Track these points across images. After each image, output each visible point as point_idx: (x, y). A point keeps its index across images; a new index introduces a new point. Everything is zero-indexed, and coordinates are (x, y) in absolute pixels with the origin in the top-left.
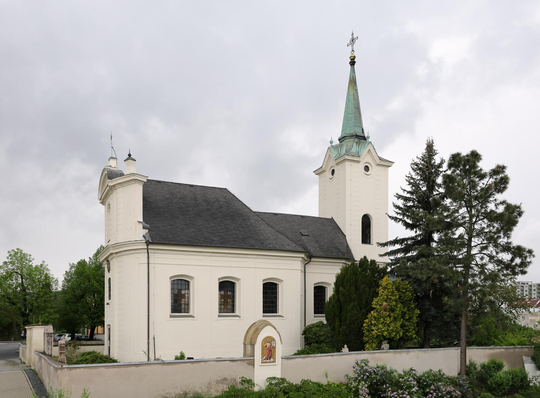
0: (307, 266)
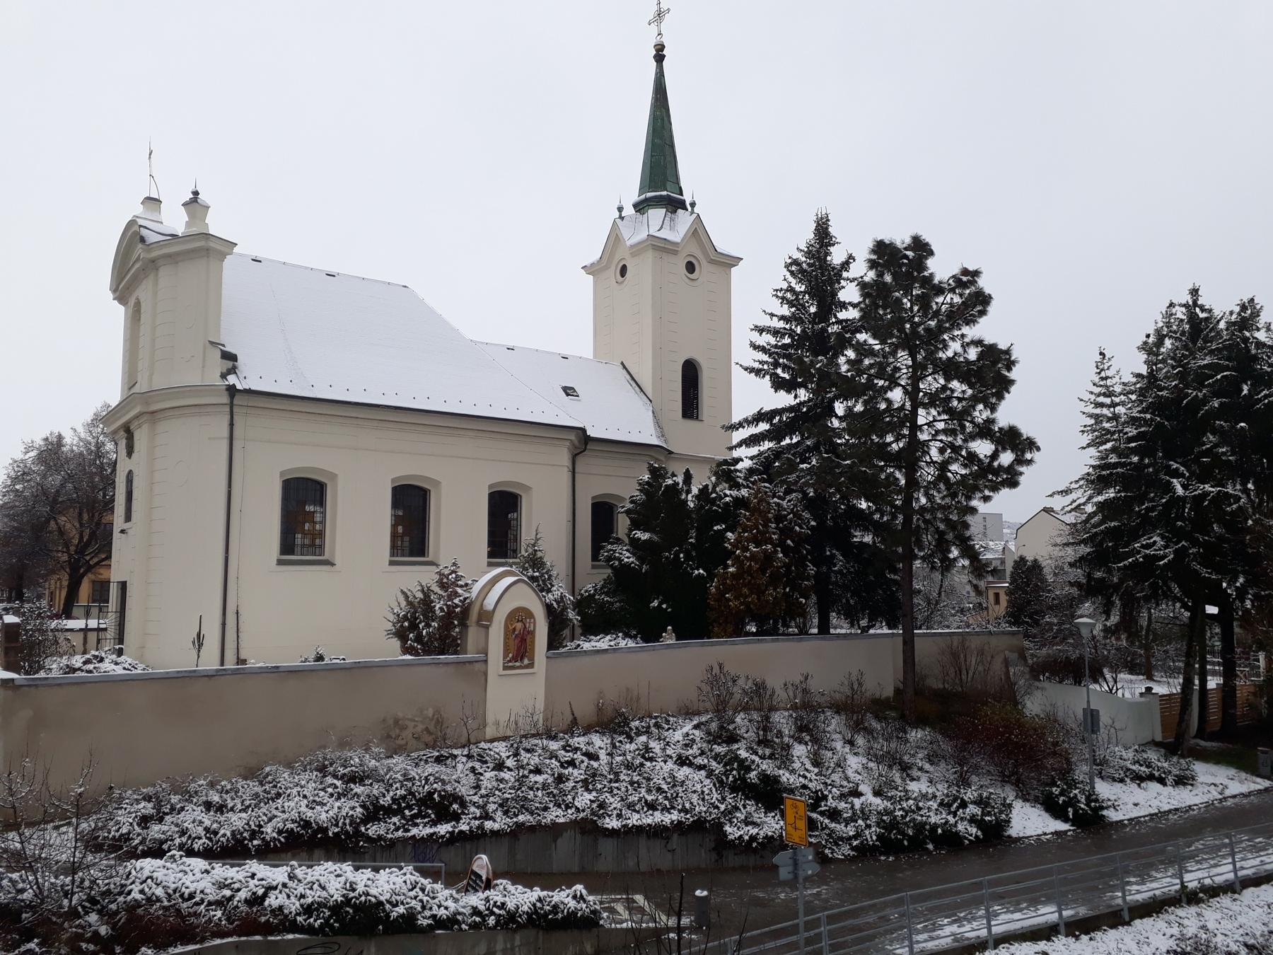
0: (580, 460)
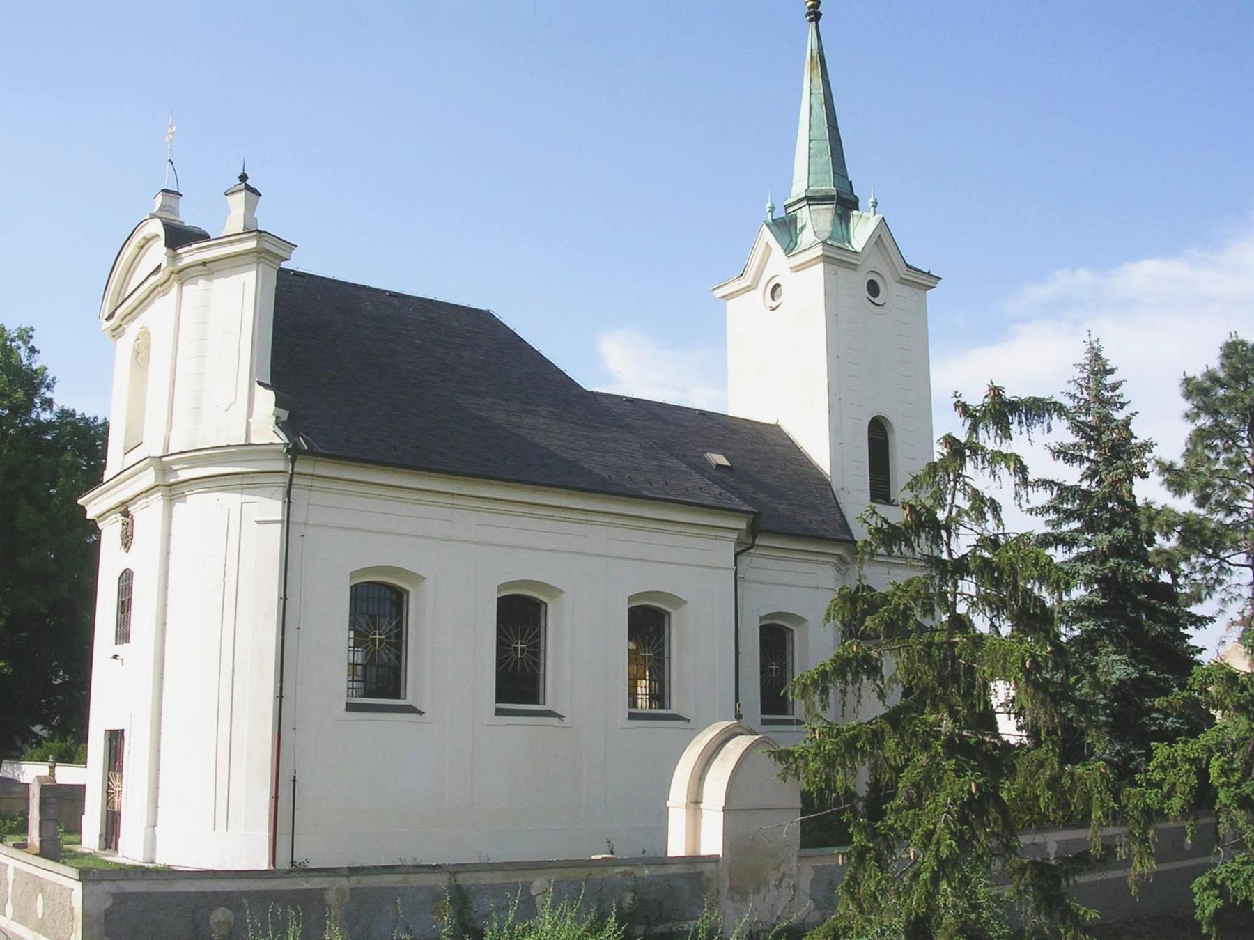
0: (740, 557)
